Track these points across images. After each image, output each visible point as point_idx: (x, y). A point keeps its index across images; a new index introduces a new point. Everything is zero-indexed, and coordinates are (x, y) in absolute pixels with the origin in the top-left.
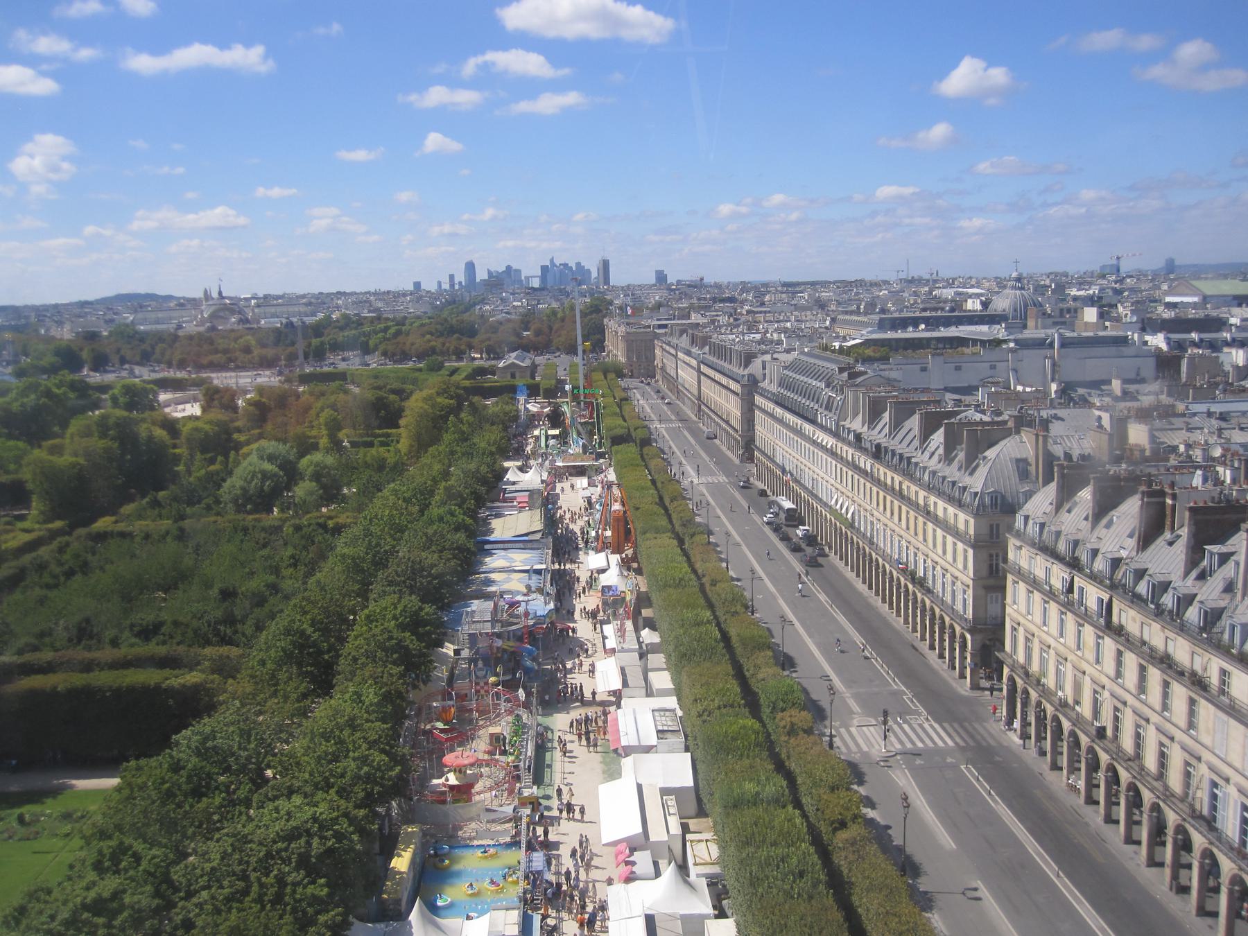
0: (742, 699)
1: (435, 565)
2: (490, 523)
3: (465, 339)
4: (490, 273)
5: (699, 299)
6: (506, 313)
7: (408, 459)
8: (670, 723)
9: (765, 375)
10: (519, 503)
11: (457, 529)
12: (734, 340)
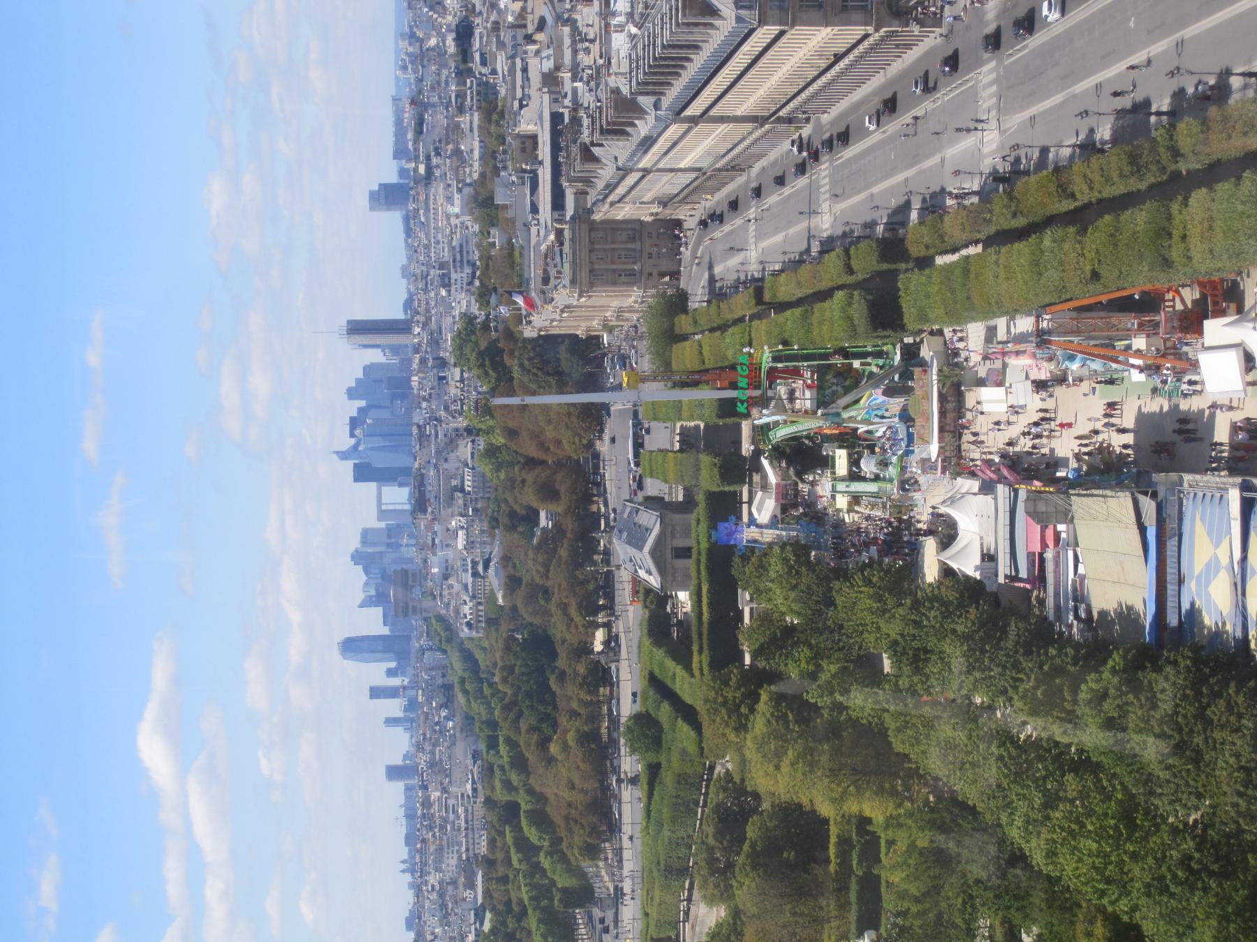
2: (1103, 614)
3: (562, 662)
4: (368, 603)
5: (461, 110)
6: (486, 567)
12: (632, 37)
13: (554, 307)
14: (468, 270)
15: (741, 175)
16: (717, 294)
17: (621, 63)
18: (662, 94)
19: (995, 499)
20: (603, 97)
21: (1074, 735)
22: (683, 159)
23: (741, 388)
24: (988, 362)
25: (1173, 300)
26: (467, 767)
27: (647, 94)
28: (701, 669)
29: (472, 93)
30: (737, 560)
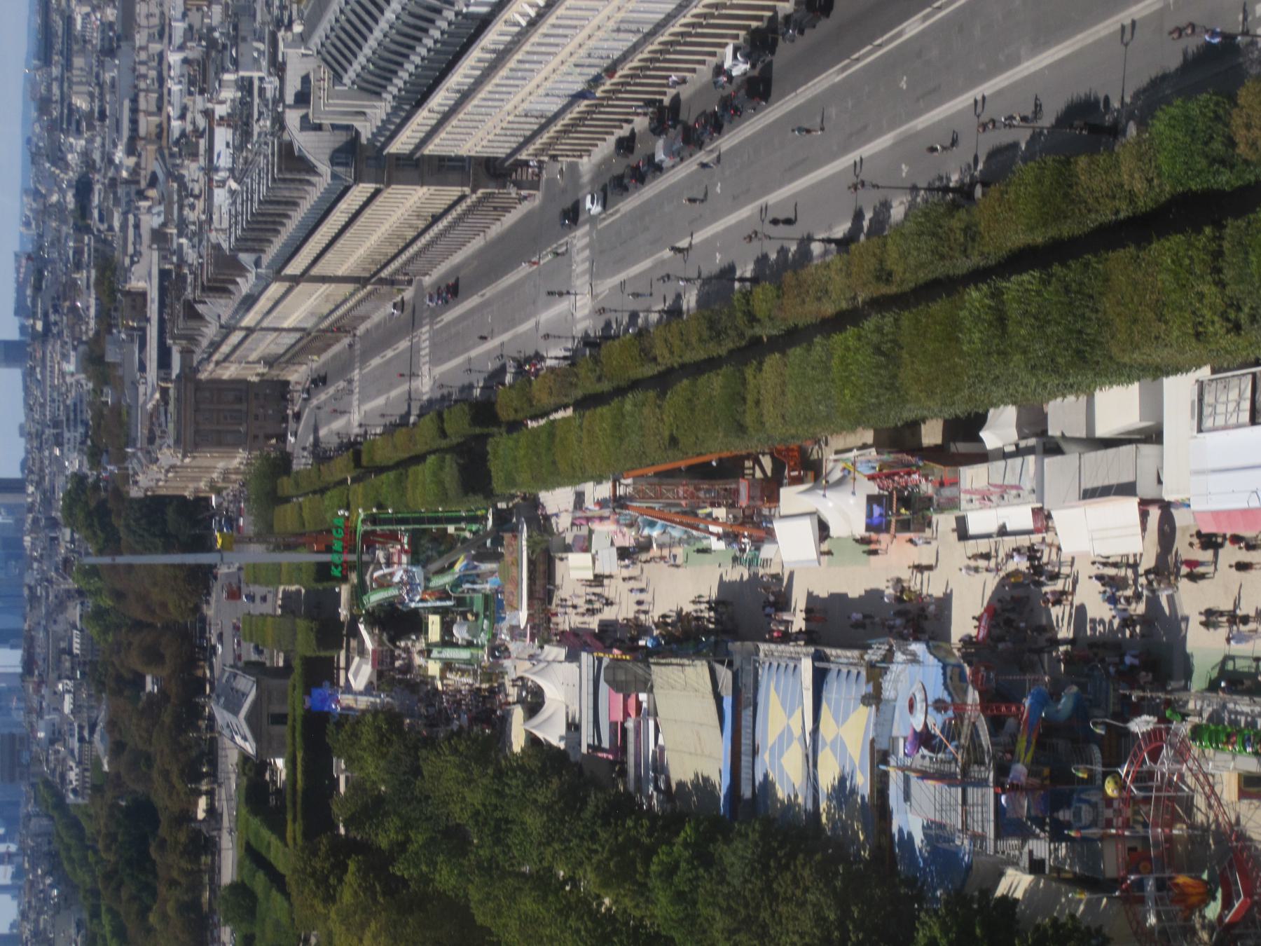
0: (1199, 231)
2: (681, 785)
3: (163, 831)
5: (78, 266)
6: (92, 732)
8: (1234, 395)
12: (232, 193)
14: (81, 430)
16: (320, 455)
17: (222, 217)
18: (263, 251)
19: (580, 667)
20: (204, 252)
21: (647, 908)
22: (286, 318)
24: (575, 528)
25: (753, 468)
27: (247, 250)
28: (295, 839)
30: (331, 727)
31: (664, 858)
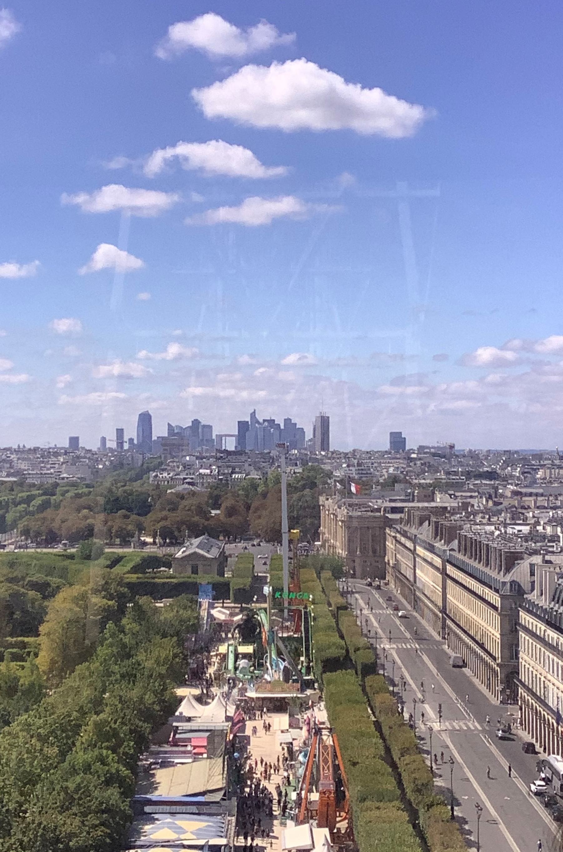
1: (75, 835)
2: (153, 775)
3: (134, 517)
5: (448, 473)
6: (189, 483)
7: (48, 679)
9: (533, 583)
10: (195, 747)
11: (108, 783)
12: (492, 533)
13: (336, 510)
15: (411, 607)
22: (422, 571)
23: (289, 594)
26: (76, 474)
29: (457, 479)
30: (190, 596)
31: (111, 758)
